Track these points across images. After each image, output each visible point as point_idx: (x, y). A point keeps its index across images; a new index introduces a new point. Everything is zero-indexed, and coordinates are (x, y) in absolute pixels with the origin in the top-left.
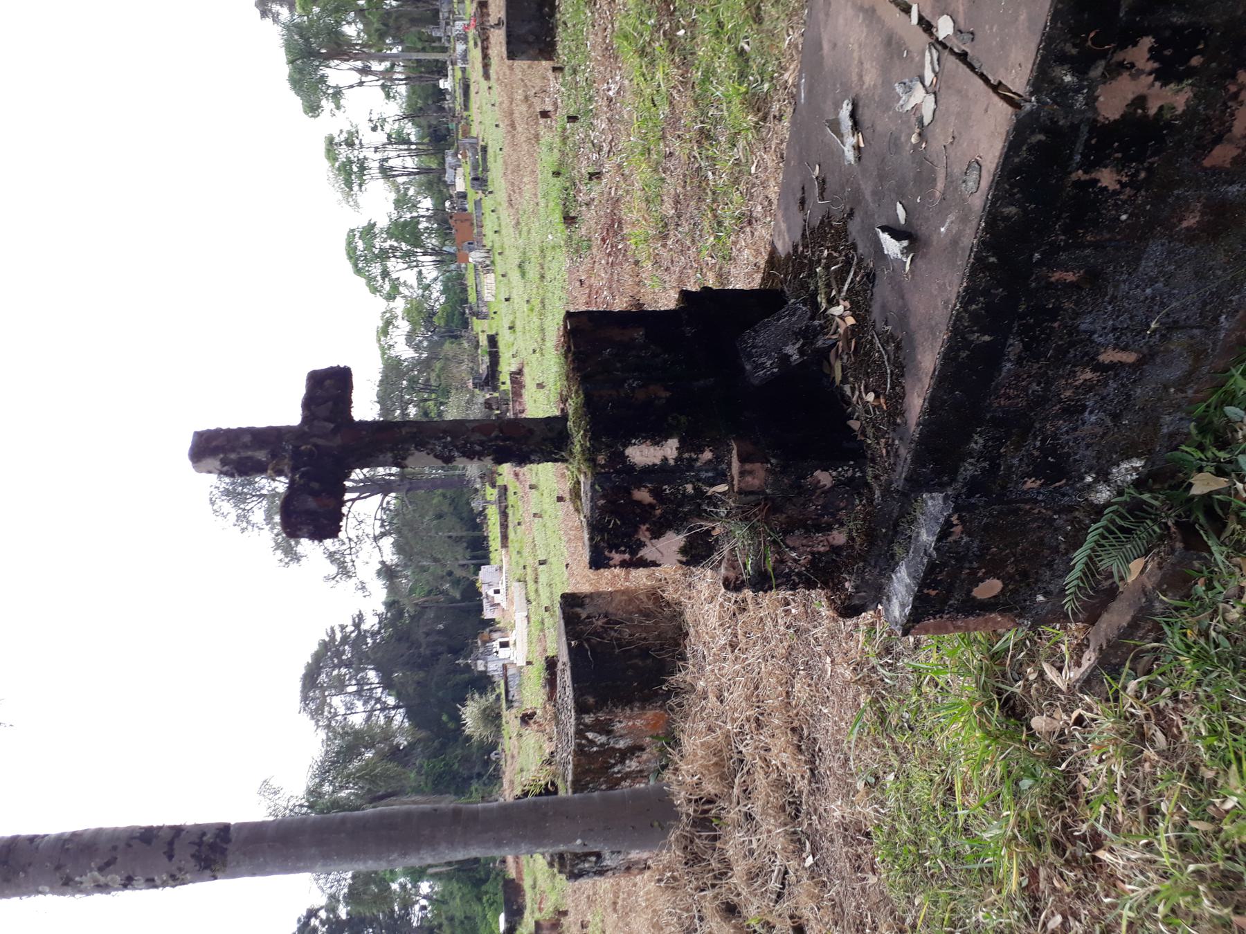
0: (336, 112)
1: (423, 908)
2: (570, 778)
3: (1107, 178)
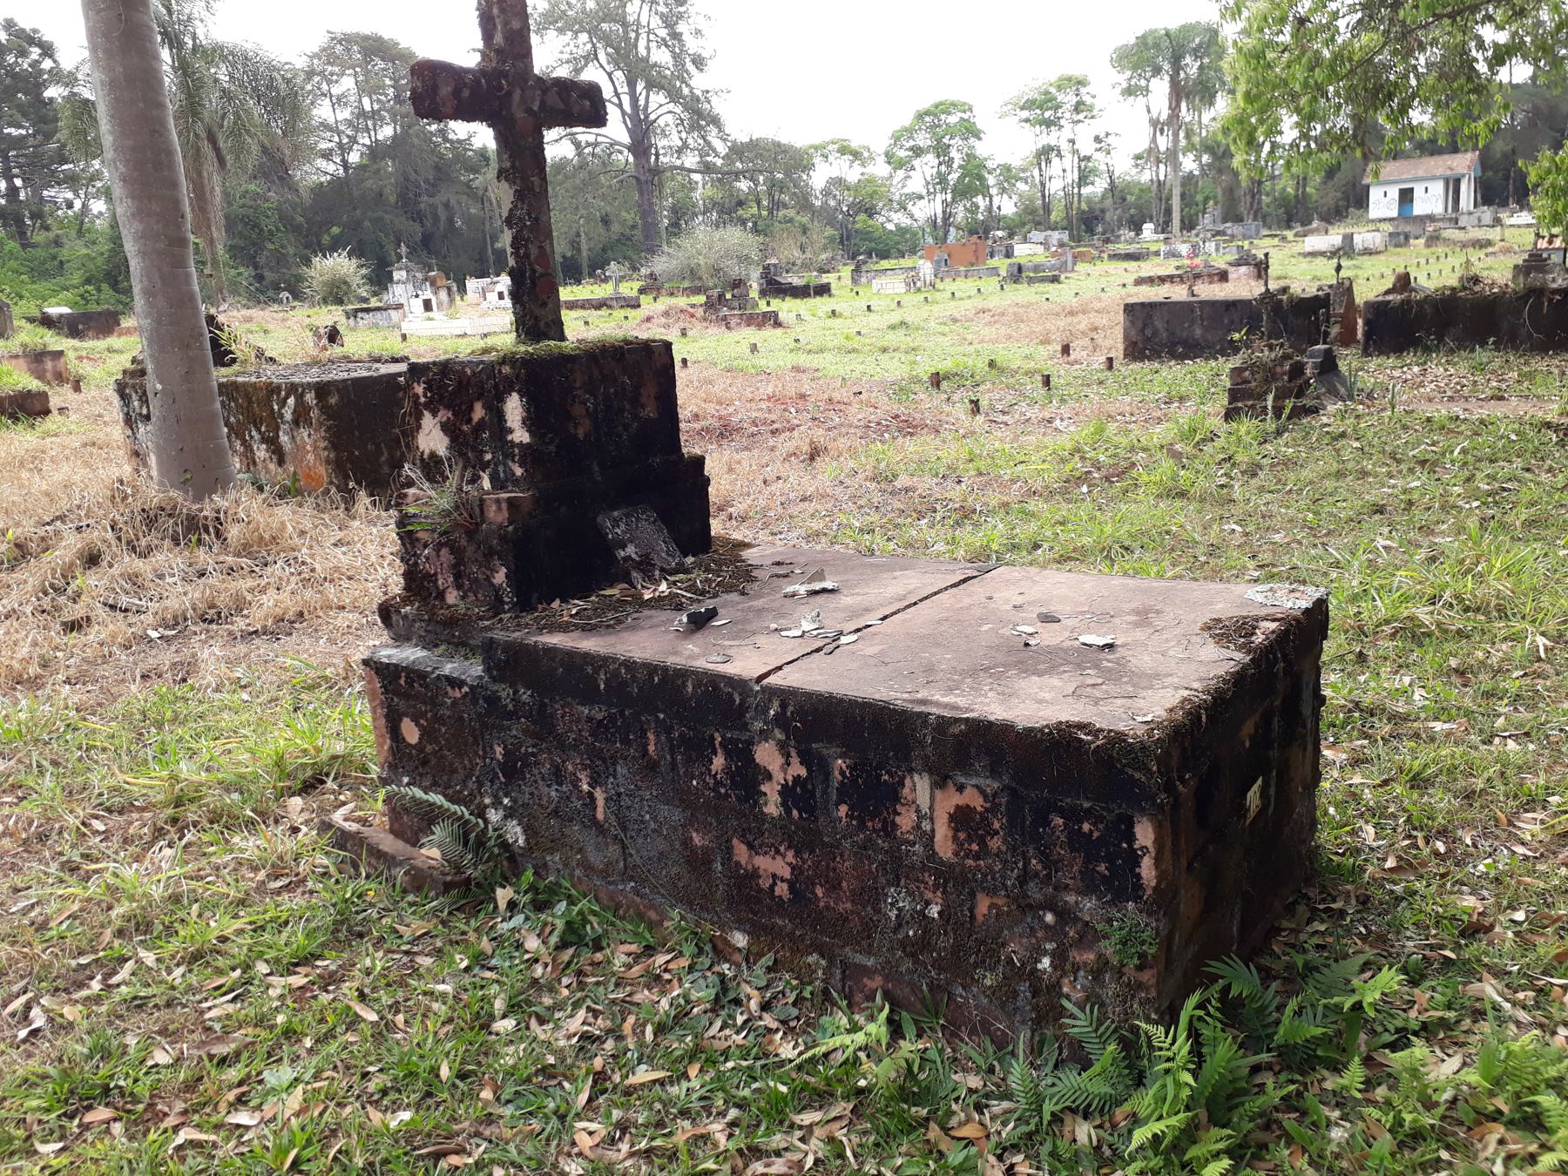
0: (1119, 90)
1: (70, 205)
2: (240, 379)
3: (718, 762)
